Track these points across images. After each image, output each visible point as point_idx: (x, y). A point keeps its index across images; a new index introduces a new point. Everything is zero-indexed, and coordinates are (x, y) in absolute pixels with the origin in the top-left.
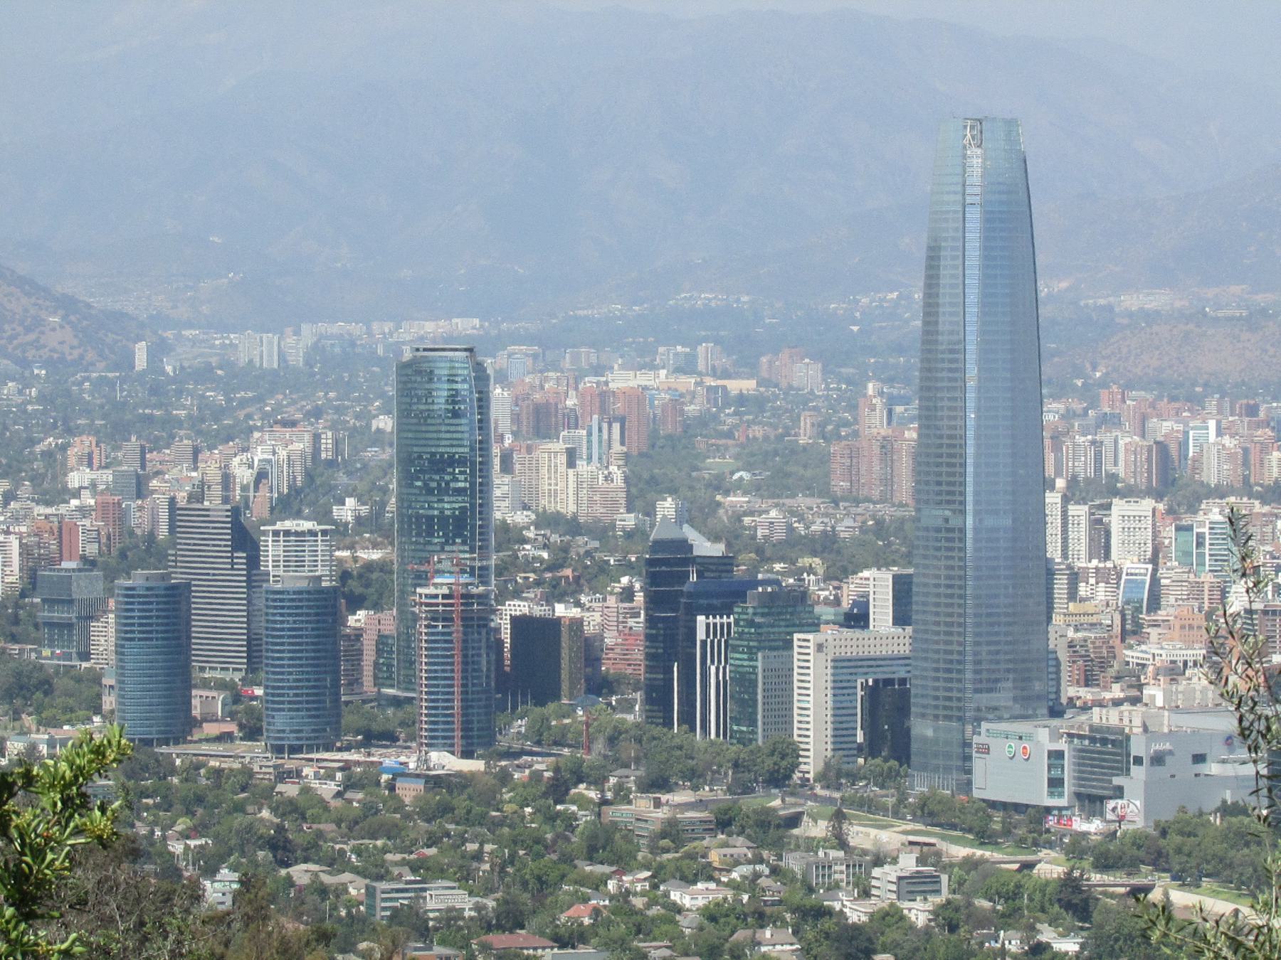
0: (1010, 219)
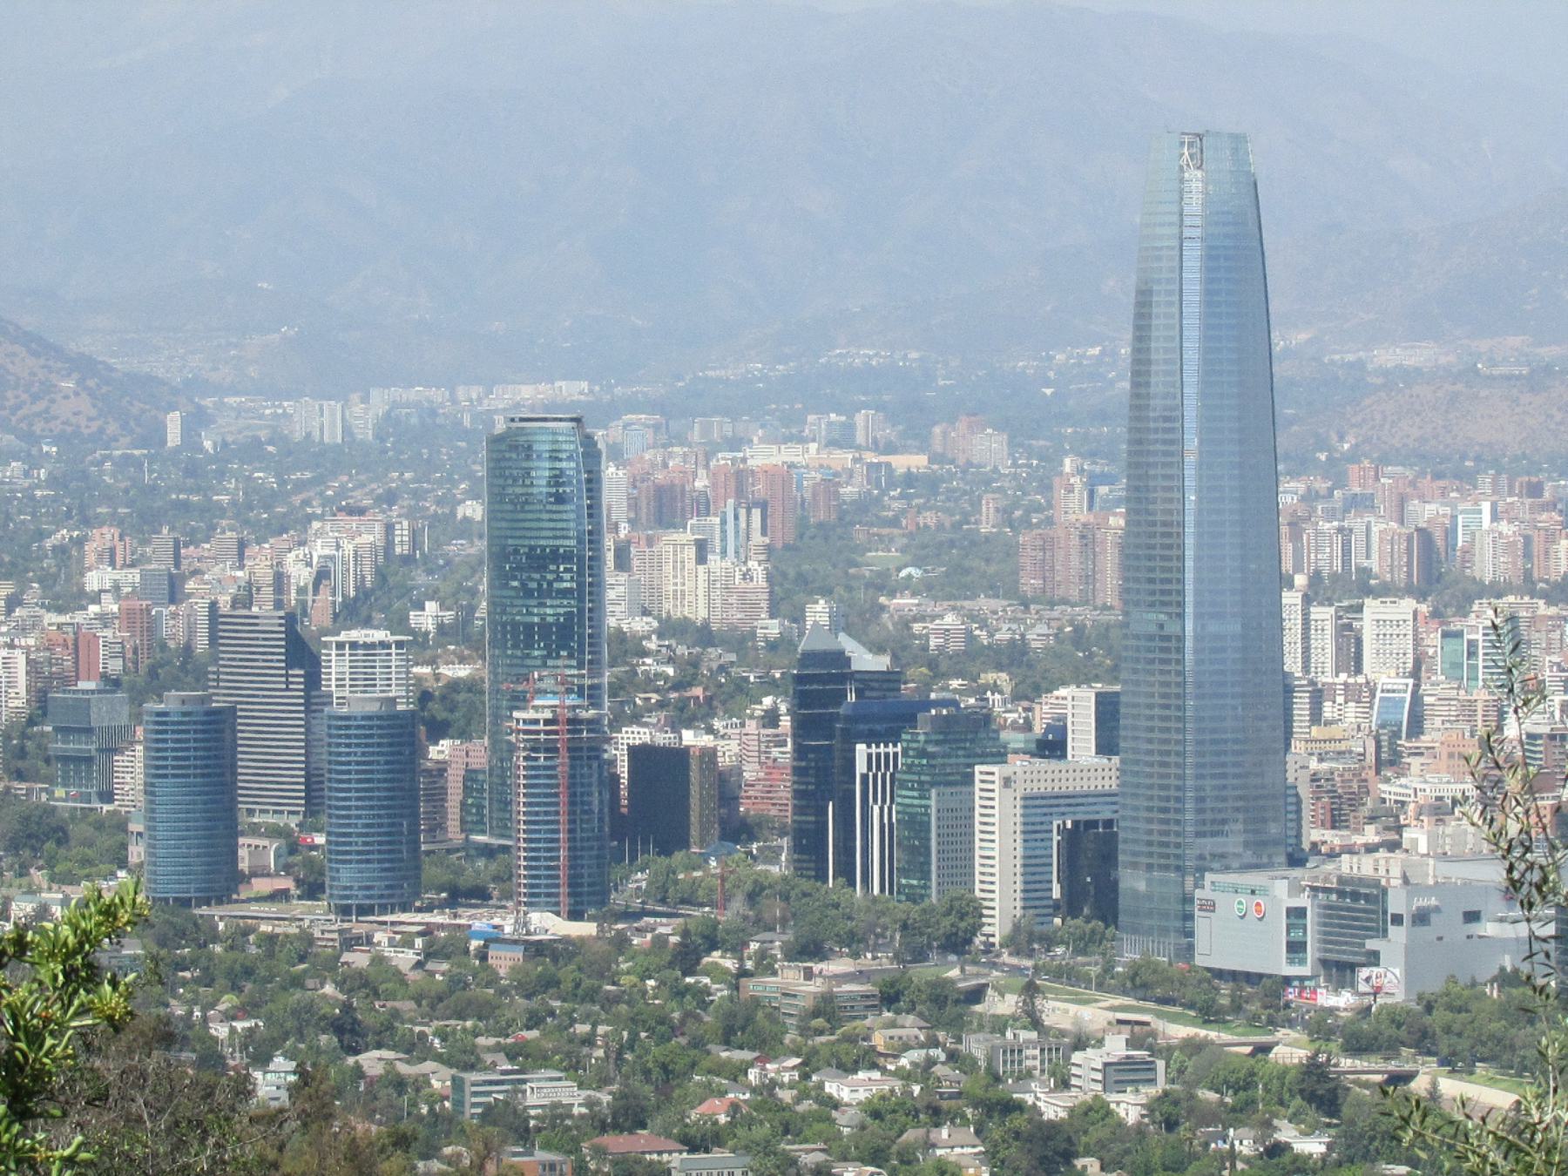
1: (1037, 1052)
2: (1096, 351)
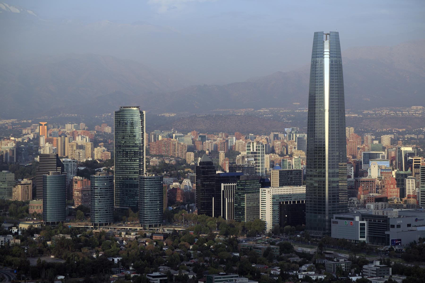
0: (121, 121)
2: (110, 114)
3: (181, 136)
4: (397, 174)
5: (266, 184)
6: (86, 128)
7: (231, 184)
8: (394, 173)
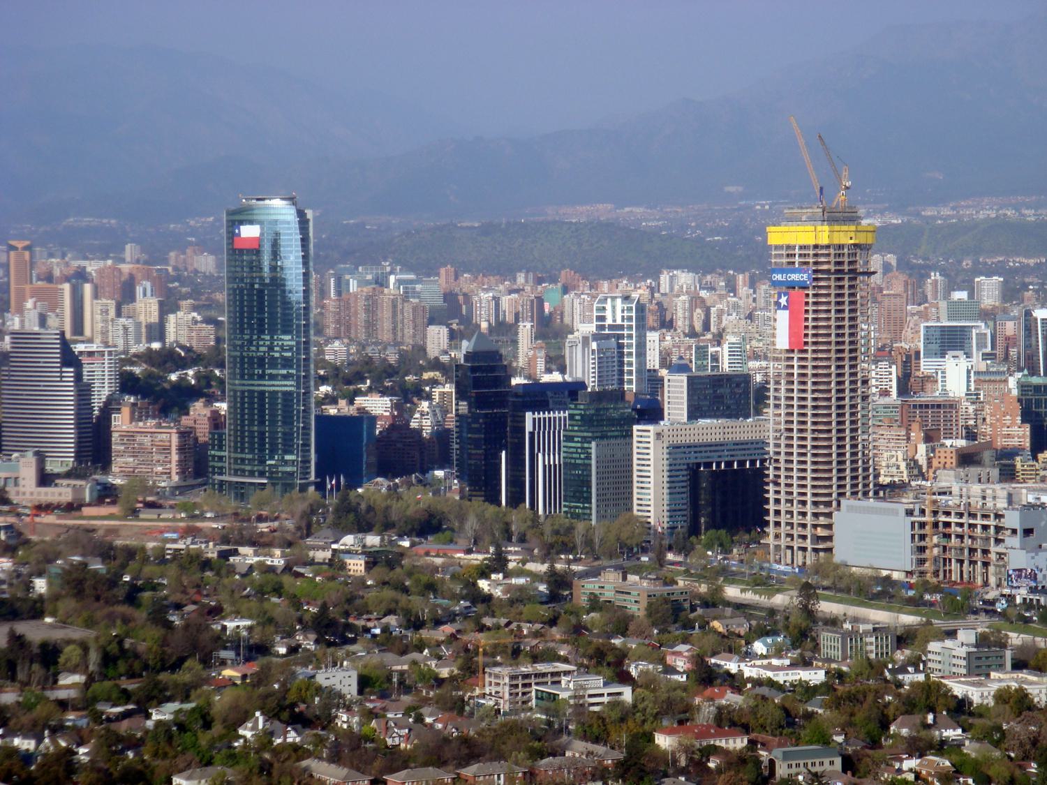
1: (873, 639)
2: (211, 219)
3: (411, 282)
4: (1023, 387)
5: (651, 412)
6: (144, 256)
7: (541, 415)
8: (1012, 382)
